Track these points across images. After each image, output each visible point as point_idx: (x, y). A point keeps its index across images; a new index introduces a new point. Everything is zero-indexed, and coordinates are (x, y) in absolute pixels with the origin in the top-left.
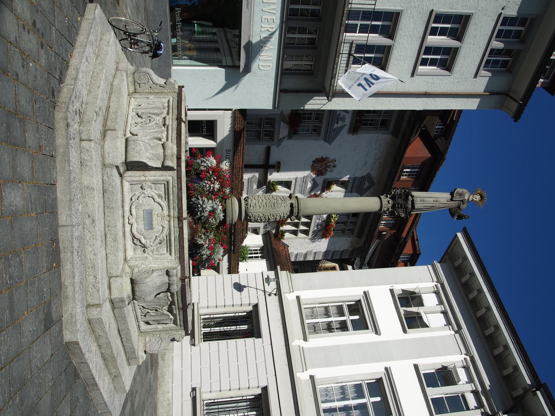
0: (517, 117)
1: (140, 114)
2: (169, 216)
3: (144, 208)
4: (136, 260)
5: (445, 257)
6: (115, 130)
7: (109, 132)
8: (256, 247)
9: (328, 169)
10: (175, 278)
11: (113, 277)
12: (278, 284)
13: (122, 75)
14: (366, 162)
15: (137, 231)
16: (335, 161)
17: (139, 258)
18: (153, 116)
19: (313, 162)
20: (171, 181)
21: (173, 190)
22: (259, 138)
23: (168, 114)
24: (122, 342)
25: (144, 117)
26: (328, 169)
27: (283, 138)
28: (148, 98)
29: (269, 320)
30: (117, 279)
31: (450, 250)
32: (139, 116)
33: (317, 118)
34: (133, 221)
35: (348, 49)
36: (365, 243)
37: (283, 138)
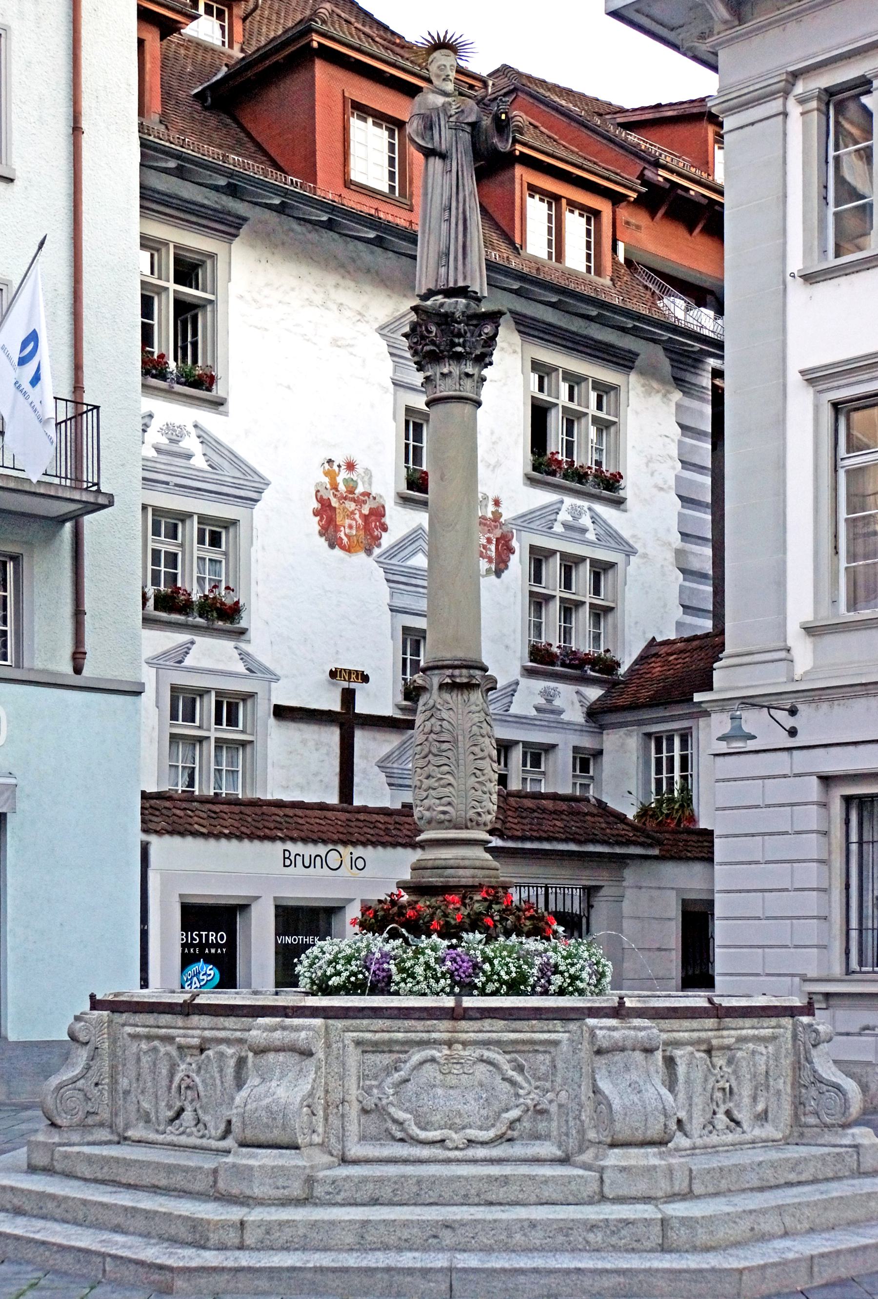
1: (171, 1114)
2: (450, 1044)
4: (567, 1135)
7: (221, 1185)
8: (647, 763)
9: (360, 489)
11: (602, 1191)
12: (750, 702)
14: (335, 343)
15: (487, 1129)
16: (330, 461)
17: (559, 1127)
18: (177, 1080)
19: (332, 546)
20: (355, 1034)
21: (375, 1031)
23: (170, 1039)
24: (800, 1183)
25: (179, 1104)
26: (360, 489)
27: (244, 656)
28: (127, 1093)
30: (607, 1181)
34: (457, 1138)
37: (244, 656)
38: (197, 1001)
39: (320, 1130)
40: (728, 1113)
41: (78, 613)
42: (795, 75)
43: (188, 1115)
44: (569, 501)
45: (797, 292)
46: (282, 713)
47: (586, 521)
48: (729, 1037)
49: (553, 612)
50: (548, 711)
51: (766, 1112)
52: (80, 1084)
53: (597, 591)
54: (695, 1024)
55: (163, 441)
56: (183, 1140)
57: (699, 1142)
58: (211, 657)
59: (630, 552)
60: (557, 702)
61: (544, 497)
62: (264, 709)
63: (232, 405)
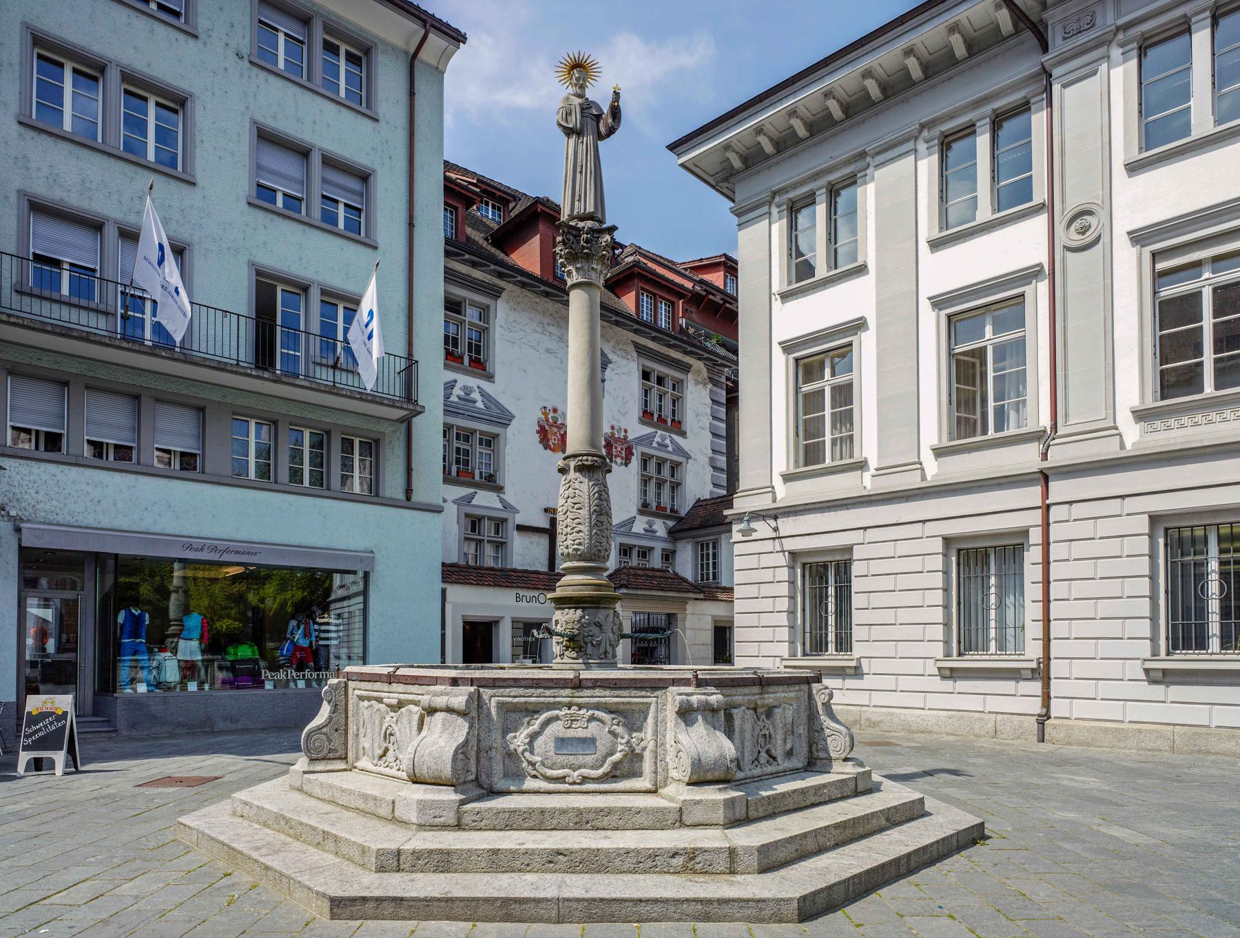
0: (457, 38)
1: (381, 752)
3: (552, 753)
5: (725, 190)
6: (393, 802)
7: (397, 813)
10: (694, 699)
13: (309, 781)
14: (548, 351)
22: (502, 544)
29: (816, 533)
31: (710, 180)
32: (384, 754)
33: (467, 439)
35: (324, 370)
36: (700, 359)
37: (502, 501)
38: (398, 673)
39: (474, 770)
40: (768, 752)
41: (409, 470)
42: (774, 194)
43: (390, 754)
44: (660, 432)
45: (776, 303)
46: (520, 528)
47: (668, 442)
48: (770, 699)
49: (652, 486)
50: (650, 532)
51: (792, 749)
52: (324, 730)
53: (673, 476)
54: (746, 690)
55: (462, 394)
56: (387, 771)
57: (749, 774)
58: (485, 500)
59: (688, 457)
60: (654, 527)
61: (647, 430)
62: (511, 526)
63: (497, 378)
